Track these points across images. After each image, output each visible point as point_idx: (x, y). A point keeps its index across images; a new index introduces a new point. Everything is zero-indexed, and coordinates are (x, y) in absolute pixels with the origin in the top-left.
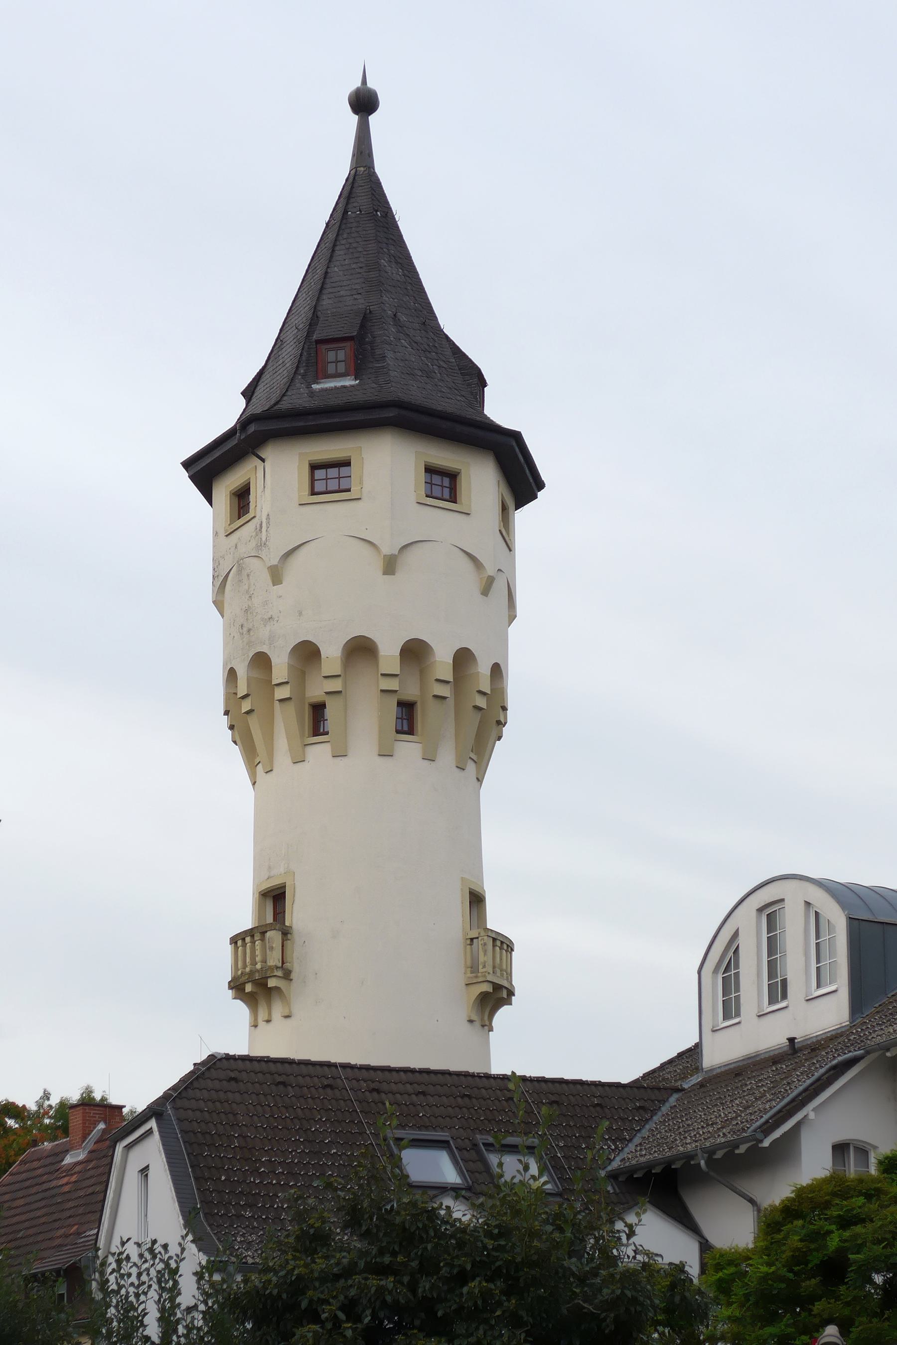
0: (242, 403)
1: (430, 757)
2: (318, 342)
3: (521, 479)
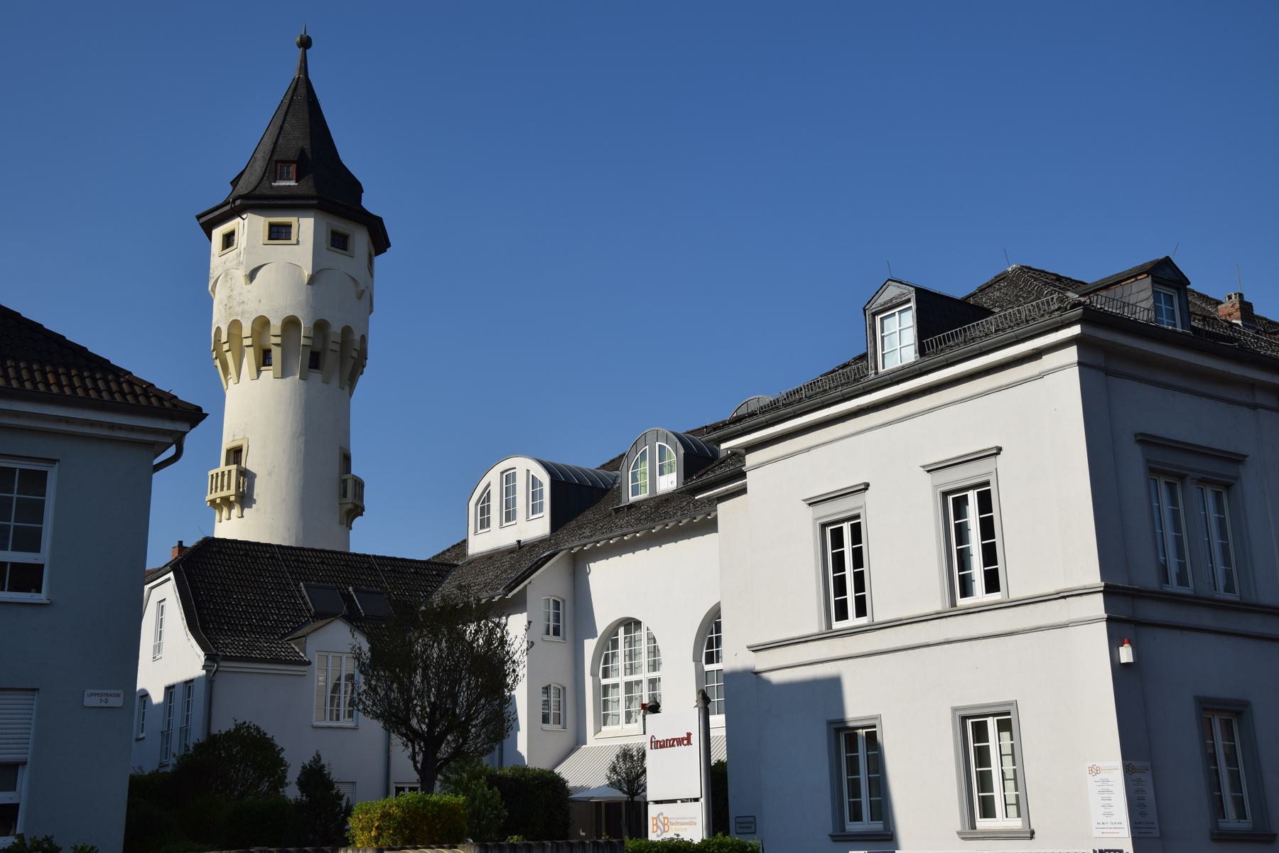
0: (231, 188)
1: (326, 381)
2: (277, 162)
3: (380, 242)
